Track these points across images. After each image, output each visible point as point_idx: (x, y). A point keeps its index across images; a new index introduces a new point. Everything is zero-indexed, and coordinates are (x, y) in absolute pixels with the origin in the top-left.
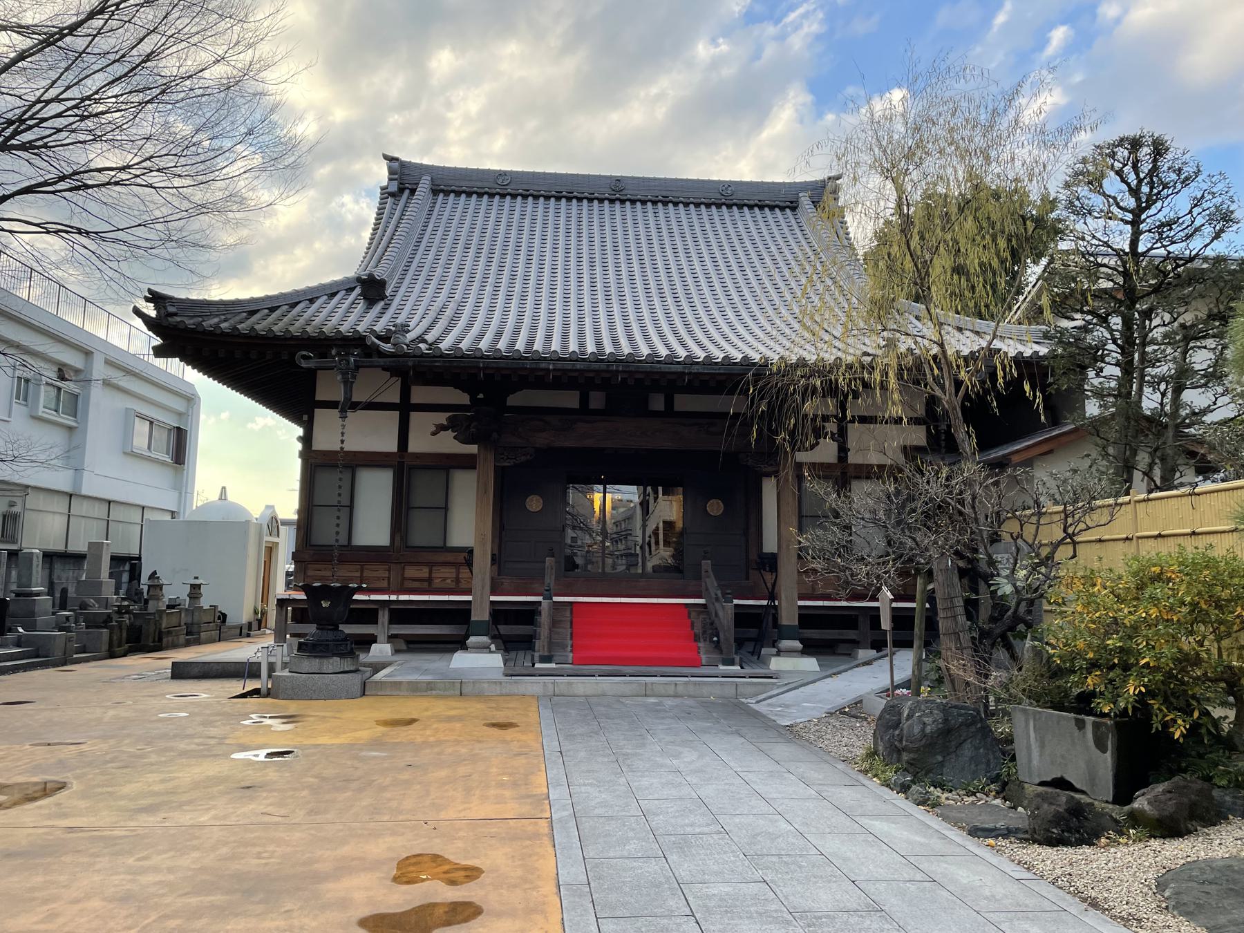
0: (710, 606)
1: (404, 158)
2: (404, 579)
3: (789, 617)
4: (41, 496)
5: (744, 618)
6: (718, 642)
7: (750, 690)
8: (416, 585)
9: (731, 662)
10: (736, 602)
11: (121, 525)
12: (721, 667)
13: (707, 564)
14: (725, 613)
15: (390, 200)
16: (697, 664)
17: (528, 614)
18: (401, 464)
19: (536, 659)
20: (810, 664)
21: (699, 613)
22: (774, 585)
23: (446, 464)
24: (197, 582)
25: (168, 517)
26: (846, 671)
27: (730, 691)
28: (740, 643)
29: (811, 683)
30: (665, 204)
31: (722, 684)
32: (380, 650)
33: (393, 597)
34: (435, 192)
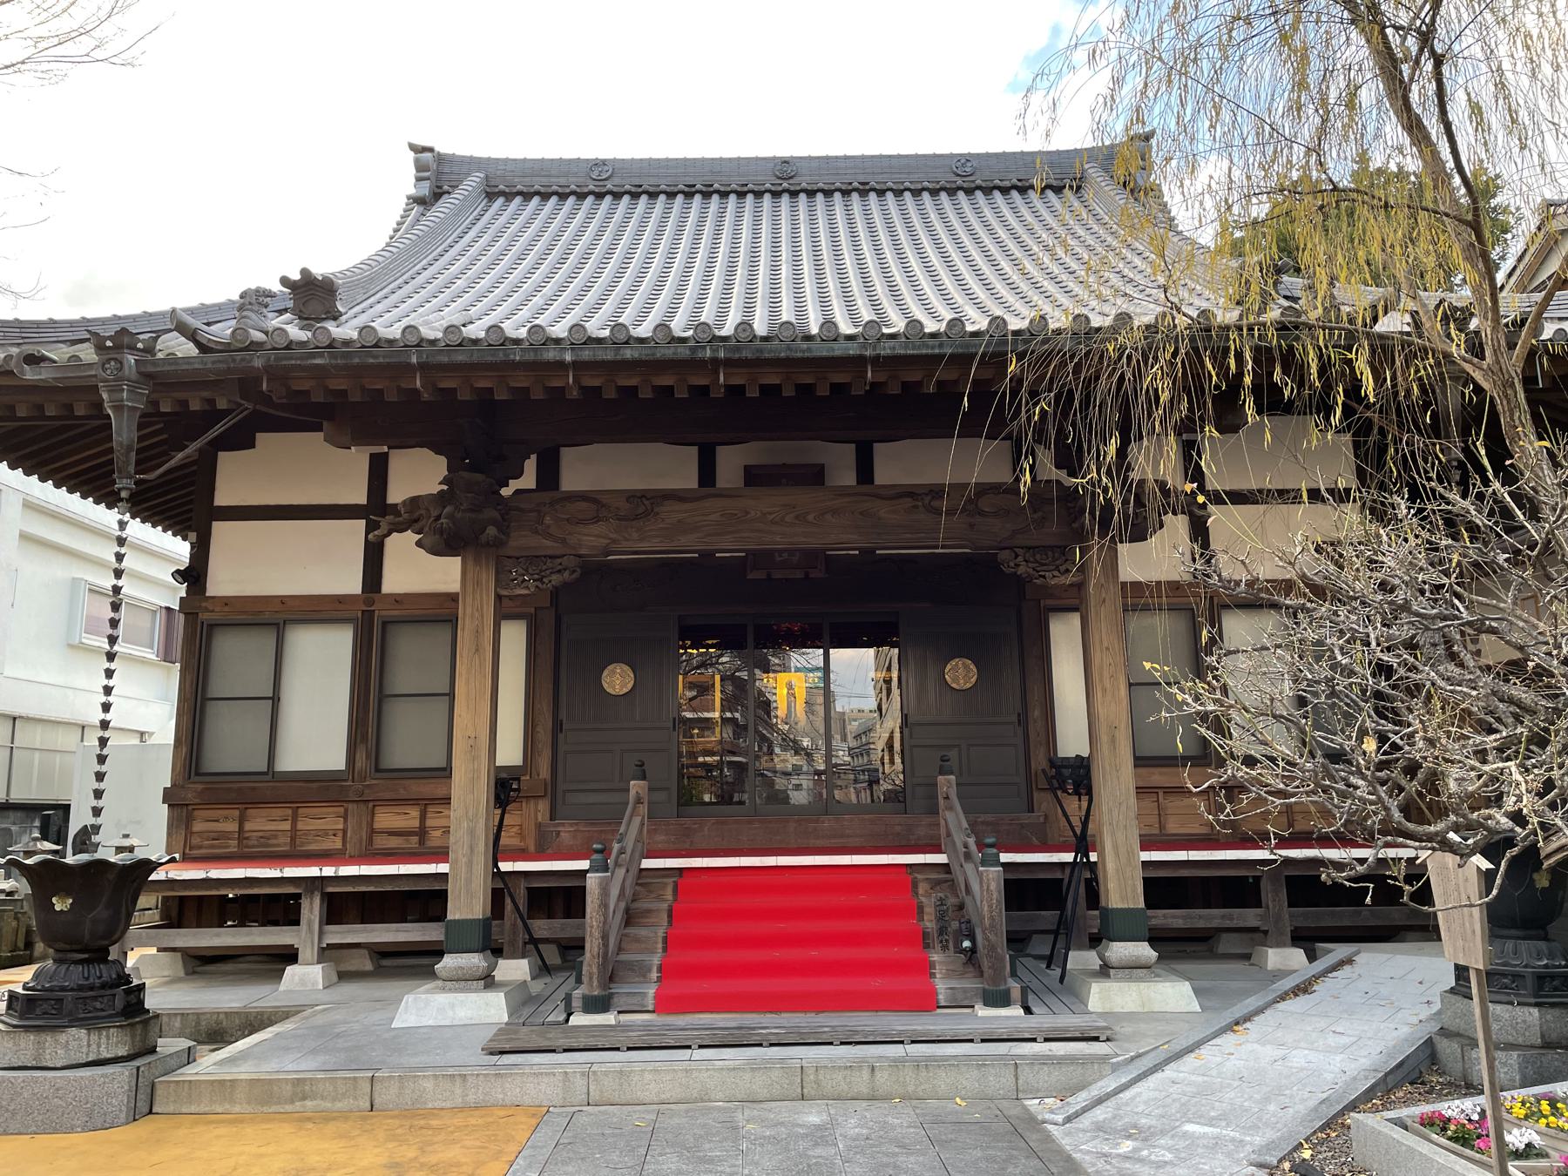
0: (955, 868)
1: (442, 148)
2: (372, 832)
3: (1123, 890)
4: (39, 728)
5: (1025, 891)
6: (973, 950)
7: (1047, 1077)
8: (394, 842)
9: (1002, 1000)
10: (1005, 857)
11: (58, 756)
12: (982, 1011)
13: (947, 784)
14: (985, 886)
15: (417, 209)
16: (925, 1002)
17: (563, 898)
18: (368, 616)
19: (576, 1003)
20: (1174, 995)
21: (935, 884)
22: (1085, 824)
23: (438, 612)
24: (126, 843)
25: (136, 741)
26: (1260, 1011)
27: (999, 1081)
28: (1017, 941)
29: (1189, 1050)
30: (863, 193)
31: (981, 1062)
32: (305, 977)
33: (328, 871)
34: (491, 196)
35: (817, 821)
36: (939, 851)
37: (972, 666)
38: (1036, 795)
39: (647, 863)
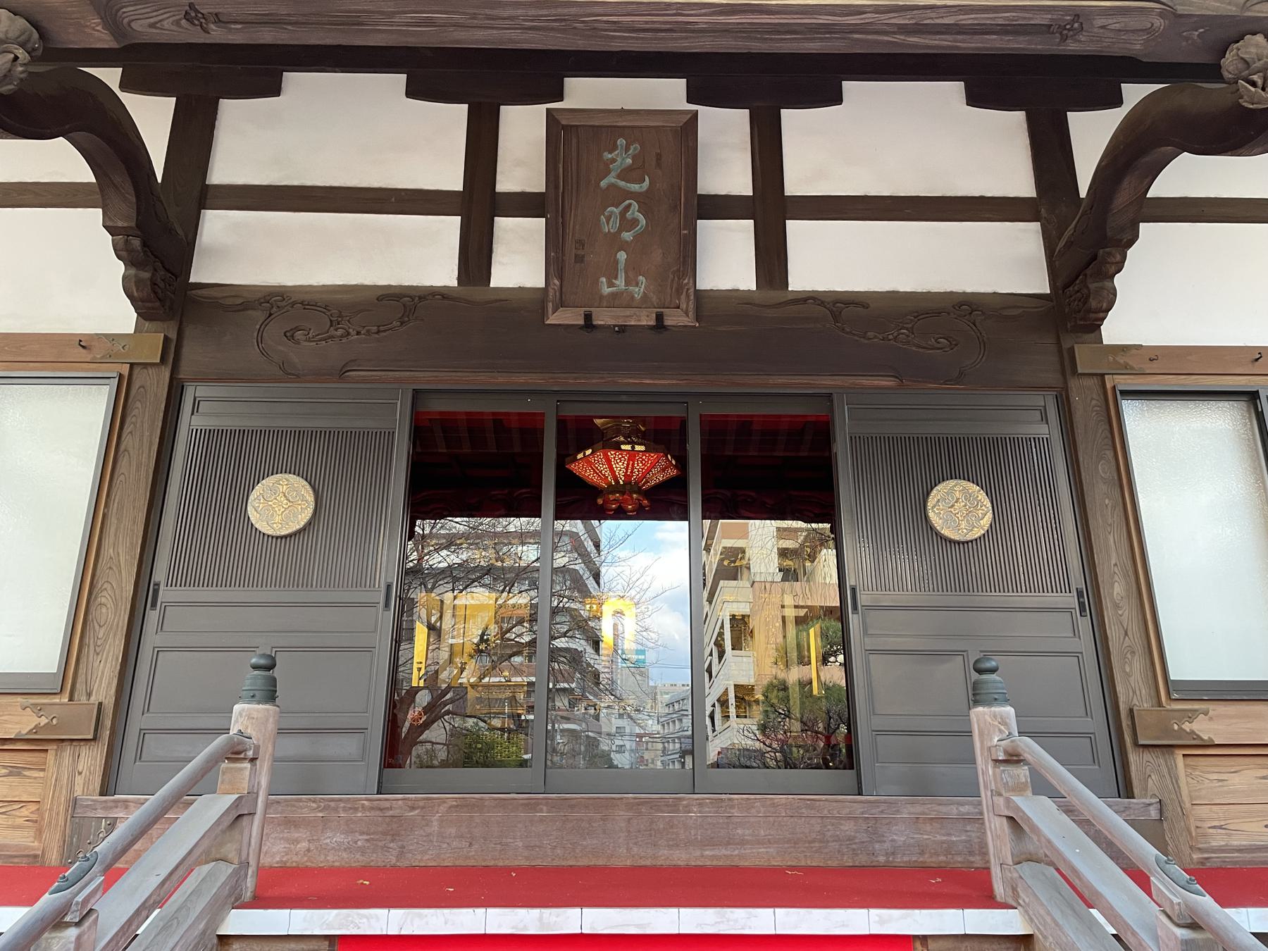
35: (674, 807)
36: (986, 899)
37: (982, 496)
38: (1133, 757)
39: (241, 922)
